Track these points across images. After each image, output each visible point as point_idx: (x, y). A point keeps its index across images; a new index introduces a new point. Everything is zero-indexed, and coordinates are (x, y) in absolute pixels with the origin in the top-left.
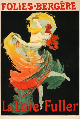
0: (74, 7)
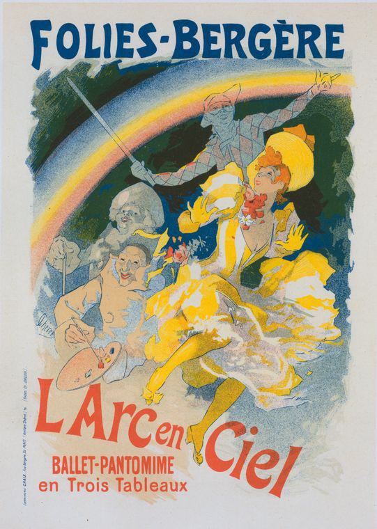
0: (336, 47)
